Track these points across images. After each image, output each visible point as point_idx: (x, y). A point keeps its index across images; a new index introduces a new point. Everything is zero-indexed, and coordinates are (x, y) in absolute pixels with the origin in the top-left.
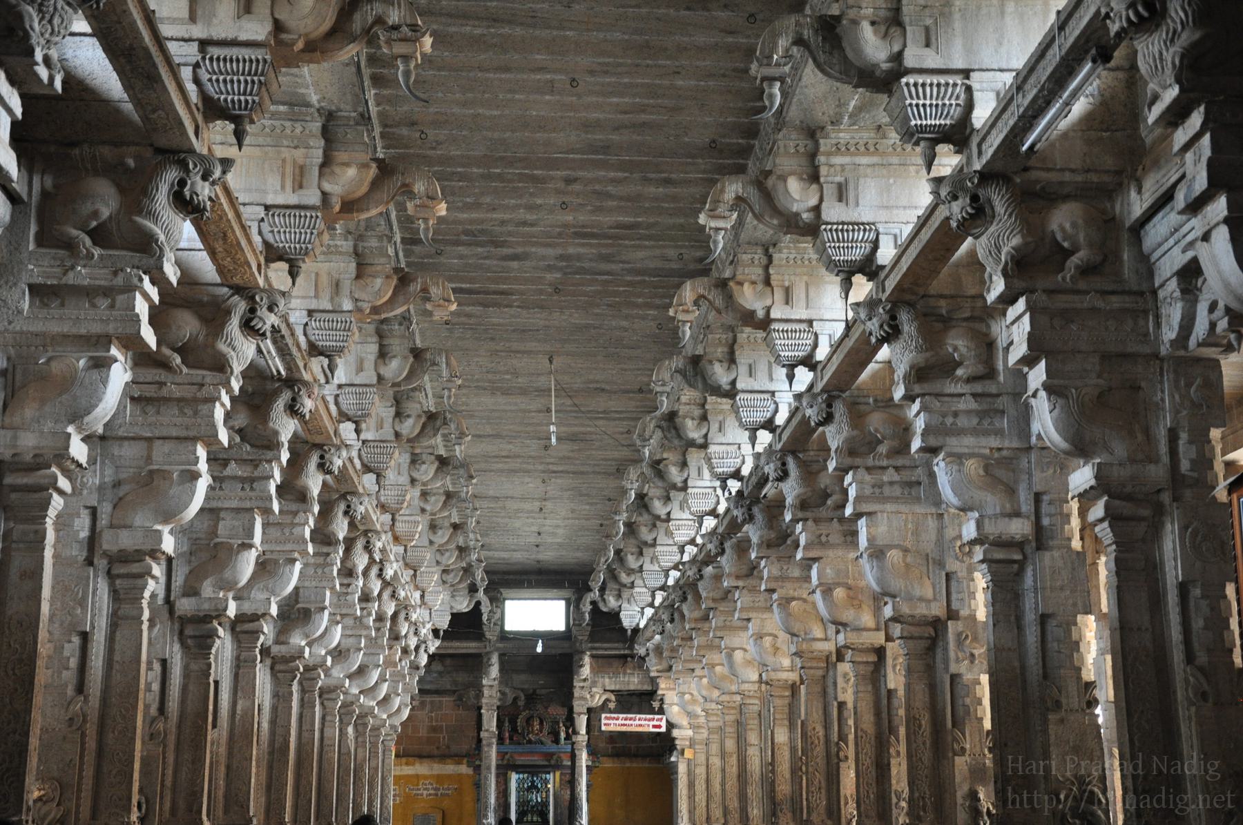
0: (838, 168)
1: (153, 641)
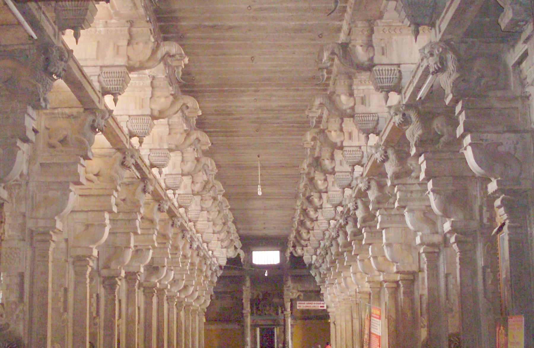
0: (362, 91)
1: (93, 288)
